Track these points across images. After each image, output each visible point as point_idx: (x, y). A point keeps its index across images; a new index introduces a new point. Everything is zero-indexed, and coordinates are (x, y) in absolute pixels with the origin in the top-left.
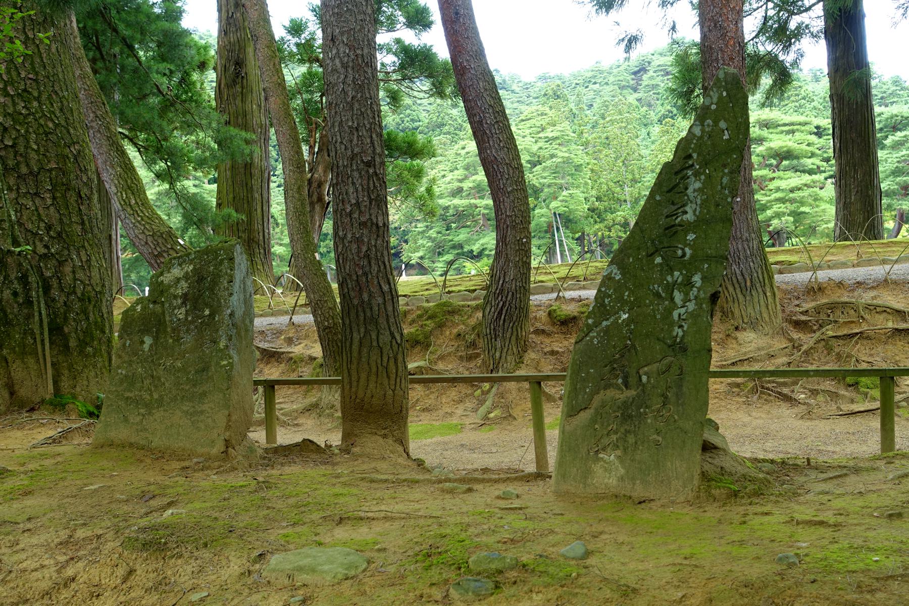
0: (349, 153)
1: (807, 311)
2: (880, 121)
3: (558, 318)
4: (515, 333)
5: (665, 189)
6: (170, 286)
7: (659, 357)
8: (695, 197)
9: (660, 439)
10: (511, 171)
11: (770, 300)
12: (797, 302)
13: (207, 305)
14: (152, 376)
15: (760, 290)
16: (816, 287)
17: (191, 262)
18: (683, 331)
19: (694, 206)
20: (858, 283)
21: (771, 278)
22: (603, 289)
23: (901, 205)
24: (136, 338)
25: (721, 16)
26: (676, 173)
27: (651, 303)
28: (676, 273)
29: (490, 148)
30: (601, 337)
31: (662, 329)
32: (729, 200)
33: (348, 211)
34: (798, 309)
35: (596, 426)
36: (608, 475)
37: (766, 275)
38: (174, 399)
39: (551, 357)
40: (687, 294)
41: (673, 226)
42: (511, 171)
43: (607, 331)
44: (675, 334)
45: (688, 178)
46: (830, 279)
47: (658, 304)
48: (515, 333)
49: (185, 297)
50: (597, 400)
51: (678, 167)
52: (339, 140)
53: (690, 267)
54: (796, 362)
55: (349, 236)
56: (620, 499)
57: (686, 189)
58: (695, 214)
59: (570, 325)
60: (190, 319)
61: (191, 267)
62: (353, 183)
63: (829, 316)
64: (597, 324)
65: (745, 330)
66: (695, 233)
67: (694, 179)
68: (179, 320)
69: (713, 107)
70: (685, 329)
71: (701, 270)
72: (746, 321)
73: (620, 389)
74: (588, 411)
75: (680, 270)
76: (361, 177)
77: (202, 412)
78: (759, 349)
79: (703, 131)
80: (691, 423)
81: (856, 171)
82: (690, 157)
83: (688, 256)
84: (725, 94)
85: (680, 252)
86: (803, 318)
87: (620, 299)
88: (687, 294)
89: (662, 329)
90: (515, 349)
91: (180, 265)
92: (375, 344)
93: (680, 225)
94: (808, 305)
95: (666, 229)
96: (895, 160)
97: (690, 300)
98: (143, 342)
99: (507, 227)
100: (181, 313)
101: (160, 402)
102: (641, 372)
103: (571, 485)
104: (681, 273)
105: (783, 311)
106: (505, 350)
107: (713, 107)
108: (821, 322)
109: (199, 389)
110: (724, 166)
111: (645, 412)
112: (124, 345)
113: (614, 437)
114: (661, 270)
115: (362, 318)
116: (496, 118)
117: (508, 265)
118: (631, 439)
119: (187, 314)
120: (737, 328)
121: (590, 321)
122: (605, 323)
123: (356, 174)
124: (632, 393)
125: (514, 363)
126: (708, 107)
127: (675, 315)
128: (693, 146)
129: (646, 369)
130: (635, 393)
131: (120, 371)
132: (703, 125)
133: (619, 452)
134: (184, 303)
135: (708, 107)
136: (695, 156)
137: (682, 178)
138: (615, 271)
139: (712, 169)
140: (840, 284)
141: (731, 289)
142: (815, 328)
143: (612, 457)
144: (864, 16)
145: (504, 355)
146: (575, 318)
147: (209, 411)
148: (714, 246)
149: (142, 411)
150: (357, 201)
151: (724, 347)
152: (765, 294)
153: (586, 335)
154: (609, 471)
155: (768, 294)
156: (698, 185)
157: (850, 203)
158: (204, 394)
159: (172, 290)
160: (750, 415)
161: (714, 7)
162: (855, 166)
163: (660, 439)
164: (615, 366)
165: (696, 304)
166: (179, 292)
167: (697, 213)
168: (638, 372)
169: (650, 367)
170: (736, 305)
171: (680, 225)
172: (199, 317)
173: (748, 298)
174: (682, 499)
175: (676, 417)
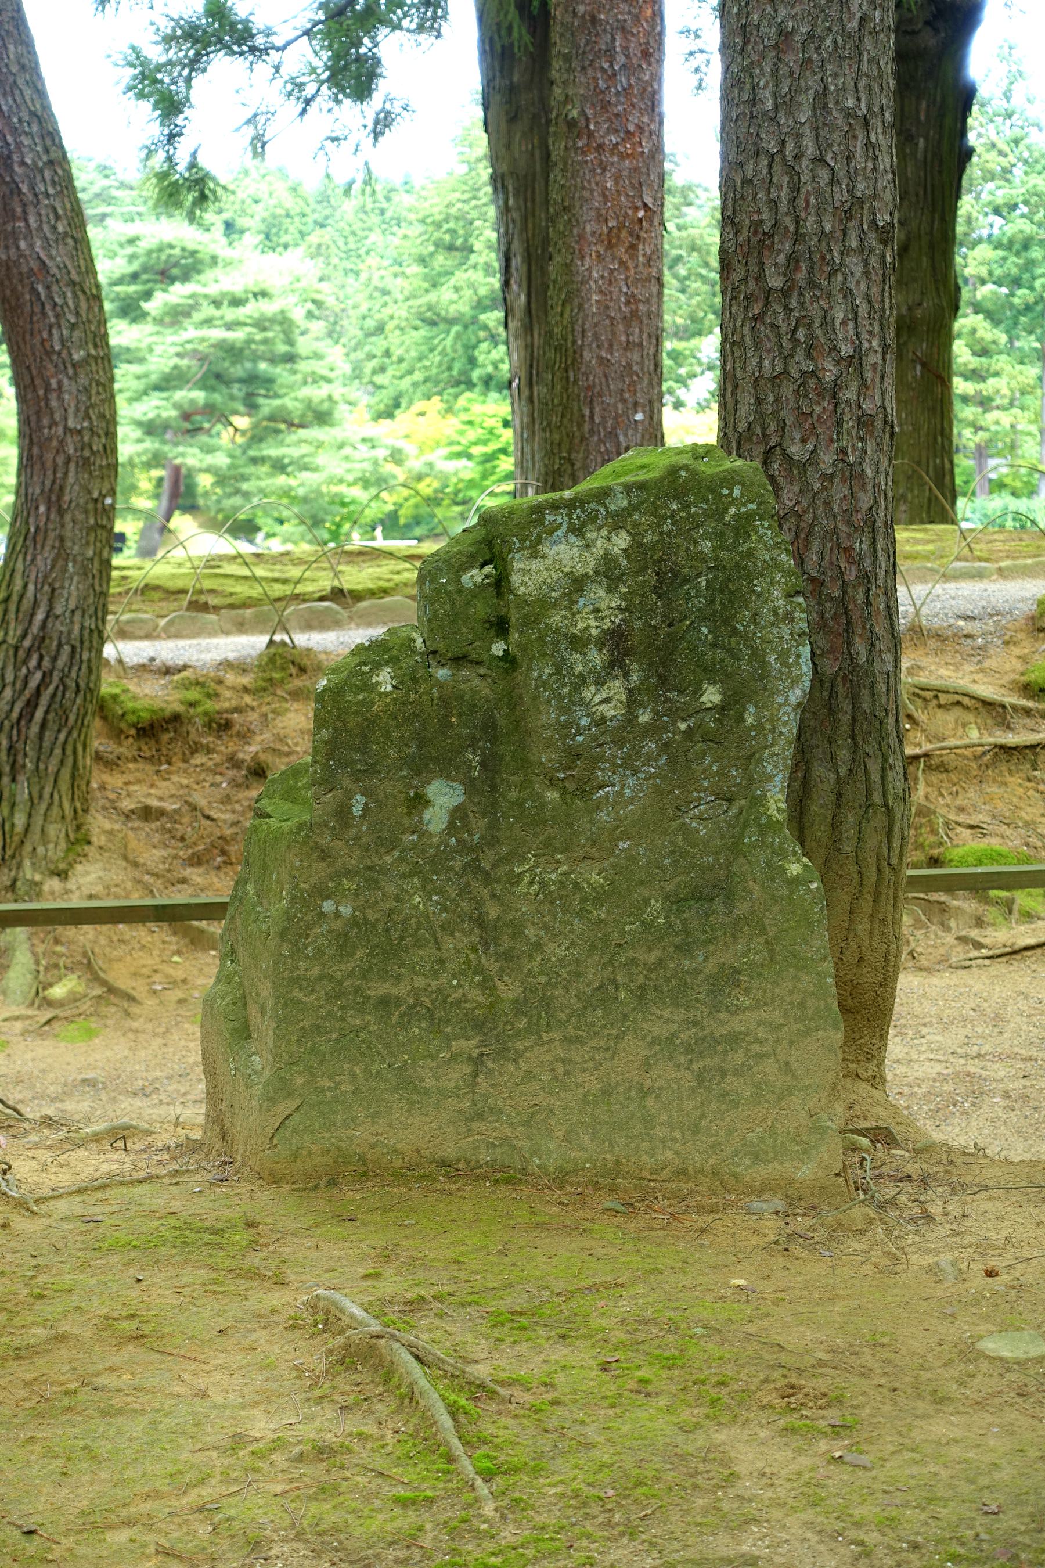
0: (840, 194)
3: (131, 718)
4: (70, 761)
6: (545, 604)
10: (83, 305)
13: (711, 673)
14: (480, 922)
17: (618, 521)
24: (392, 788)
29: (29, 234)
33: (828, 378)
38: (602, 997)
39: (147, 827)
42: (83, 305)
48: (70, 761)
49: (618, 644)
52: (811, 151)
55: (827, 459)
59: (165, 737)
60: (644, 718)
61: (622, 541)
62: (847, 292)
68: (603, 720)
76: (866, 274)
77: (734, 1040)
90: (66, 805)
91: (578, 531)
92: (877, 798)
98: (419, 802)
99: (68, 460)
100: (607, 700)
101: (537, 1009)
106: (43, 806)
109: (707, 962)
112: (343, 812)
115: (846, 719)
116: (47, 151)
117: (65, 569)
119: (633, 700)
123: (855, 264)
125: (63, 845)
131: (328, 906)
134: (616, 664)
145: (38, 820)
146: (176, 718)
147: (762, 1033)
149: (463, 1045)
150: (858, 349)
158: (729, 977)
159: (557, 618)
166: (589, 625)
172: (677, 713)
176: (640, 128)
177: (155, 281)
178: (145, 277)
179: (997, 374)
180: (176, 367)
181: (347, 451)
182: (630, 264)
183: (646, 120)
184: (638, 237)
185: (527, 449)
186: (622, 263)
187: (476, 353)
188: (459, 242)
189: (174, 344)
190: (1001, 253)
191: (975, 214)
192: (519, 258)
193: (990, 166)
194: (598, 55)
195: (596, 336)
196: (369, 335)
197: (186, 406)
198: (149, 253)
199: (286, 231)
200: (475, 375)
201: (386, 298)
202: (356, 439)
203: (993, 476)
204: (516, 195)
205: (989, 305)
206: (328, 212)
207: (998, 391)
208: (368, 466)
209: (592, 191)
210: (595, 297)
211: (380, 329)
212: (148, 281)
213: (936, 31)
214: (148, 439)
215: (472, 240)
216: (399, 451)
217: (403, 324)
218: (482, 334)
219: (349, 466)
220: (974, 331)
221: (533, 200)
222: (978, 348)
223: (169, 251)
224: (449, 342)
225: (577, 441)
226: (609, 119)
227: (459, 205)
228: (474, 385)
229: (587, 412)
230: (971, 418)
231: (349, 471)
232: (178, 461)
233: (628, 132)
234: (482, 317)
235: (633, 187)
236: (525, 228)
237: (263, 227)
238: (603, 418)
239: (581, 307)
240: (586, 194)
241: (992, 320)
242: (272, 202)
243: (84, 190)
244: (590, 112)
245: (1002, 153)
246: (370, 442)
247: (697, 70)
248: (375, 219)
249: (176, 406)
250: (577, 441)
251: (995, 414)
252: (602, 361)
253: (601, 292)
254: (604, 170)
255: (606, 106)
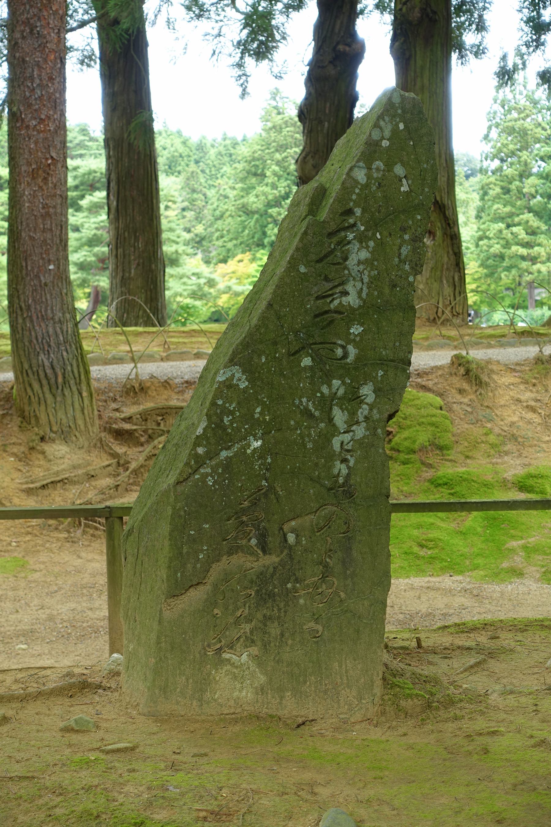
1: (130, 418)
2: (75, 177)
5: (314, 257)
7: (314, 505)
8: (361, 273)
9: (320, 628)
11: (86, 402)
12: (114, 406)
15: (74, 389)
16: (137, 386)
18: (349, 468)
19: (359, 285)
20: (187, 382)
21: (87, 372)
22: (220, 402)
23: (98, 281)
25: (39, 19)
26: (331, 235)
27: (298, 425)
28: (334, 381)
30: (219, 475)
31: (316, 465)
32: (411, 279)
34: (118, 414)
35: (216, 611)
36: (238, 686)
37: (82, 370)
40: (353, 414)
41: (326, 312)
43: (228, 465)
44: (336, 471)
45: (349, 242)
46: (152, 377)
47: (309, 427)
50: (216, 571)
51: (333, 227)
53: (357, 373)
54: (124, 485)
56: (263, 721)
57: (346, 259)
58: (360, 297)
63: (159, 424)
64: (211, 455)
65: (53, 441)
66: (362, 325)
67: (357, 245)
69: (385, 143)
70: (351, 464)
71: (374, 379)
72: (55, 429)
73: (252, 554)
74: (201, 588)
75: (341, 378)
78: (74, 467)
79: (369, 176)
80: (366, 603)
81: (137, 239)
82: (349, 212)
83: (351, 359)
84: (401, 126)
85: (339, 352)
86: (127, 426)
87: (248, 417)
88: (353, 414)
89: (316, 465)
93: (337, 312)
94: (130, 410)
95: (316, 316)
96: (93, 226)
97: (358, 423)
102: (286, 527)
103: (178, 703)
104: (343, 383)
105: (100, 417)
107: (385, 143)
108: (150, 432)
110: (404, 230)
111: (294, 588)
113: (247, 627)
114: (312, 377)
118: (274, 630)
120: (42, 439)
121: (200, 450)
122: (224, 454)
124: (274, 559)
126: (377, 144)
127: (336, 443)
128: (354, 197)
129: (293, 523)
130: (277, 560)
132: (369, 168)
133: (254, 650)
135: (377, 144)
136: (358, 212)
137: (339, 243)
138: (237, 375)
139: (385, 233)
140: (166, 384)
141: (36, 386)
142: (143, 439)
143: (244, 657)
144: (147, 45)
148: (391, 345)
151: (28, 464)
152: (80, 394)
153: (195, 471)
154: (239, 680)
155: (85, 394)
156: (364, 255)
157: (129, 278)
160: (79, 557)
161: (31, 6)
162: (135, 232)
163: (320, 628)
164: (245, 519)
165: (367, 429)
167: (364, 295)
168: (281, 529)
169: (299, 521)
170: (43, 407)
171: (337, 312)
173: (59, 399)
174: (358, 716)
175: (342, 595)
176: (49, 118)
177: (87, 190)
178: (82, 188)
179: (539, 245)
180: (95, 235)
181: (185, 280)
182: (45, 188)
183: (51, 113)
184: (48, 174)
185: (114, 282)
186: (40, 187)
187: (266, 229)
188: (259, 172)
189: (95, 223)
190: (542, 181)
191: (529, 161)
192: (114, 182)
193: (538, 135)
194: (25, 79)
195: (28, 225)
196: (217, 219)
197: (100, 255)
198: (84, 175)
199: (180, 165)
200: (266, 241)
201: (226, 200)
202: (189, 273)
203: (538, 298)
204: (114, 150)
205: (536, 208)
206: (201, 155)
207: (539, 254)
208: (194, 288)
209: (24, 149)
210: (27, 205)
211: (221, 217)
212: (83, 190)
213: (335, 66)
214: (80, 272)
215: (266, 171)
216: (213, 280)
217: (233, 214)
218: (269, 220)
219: (185, 287)
220: (528, 222)
221: (122, 153)
222: (529, 231)
223: (94, 174)
224: (252, 224)
225: (20, 279)
226: (31, 113)
227: (260, 152)
228: (266, 246)
229: (24, 264)
230: (525, 267)
231: (185, 290)
232: (96, 284)
233: (41, 119)
234: (270, 211)
235: (45, 148)
236: (117, 167)
237: (167, 162)
238: (32, 267)
239: (20, 209)
240: (21, 151)
241: (538, 216)
242: (172, 149)
243: (71, 142)
244: (22, 108)
245: (544, 129)
246: (197, 275)
247: (242, 85)
248: (227, 159)
249: (95, 255)
250: (20, 279)
251: (538, 266)
252: (31, 238)
253: (30, 202)
254: (30, 138)
255: (30, 106)
